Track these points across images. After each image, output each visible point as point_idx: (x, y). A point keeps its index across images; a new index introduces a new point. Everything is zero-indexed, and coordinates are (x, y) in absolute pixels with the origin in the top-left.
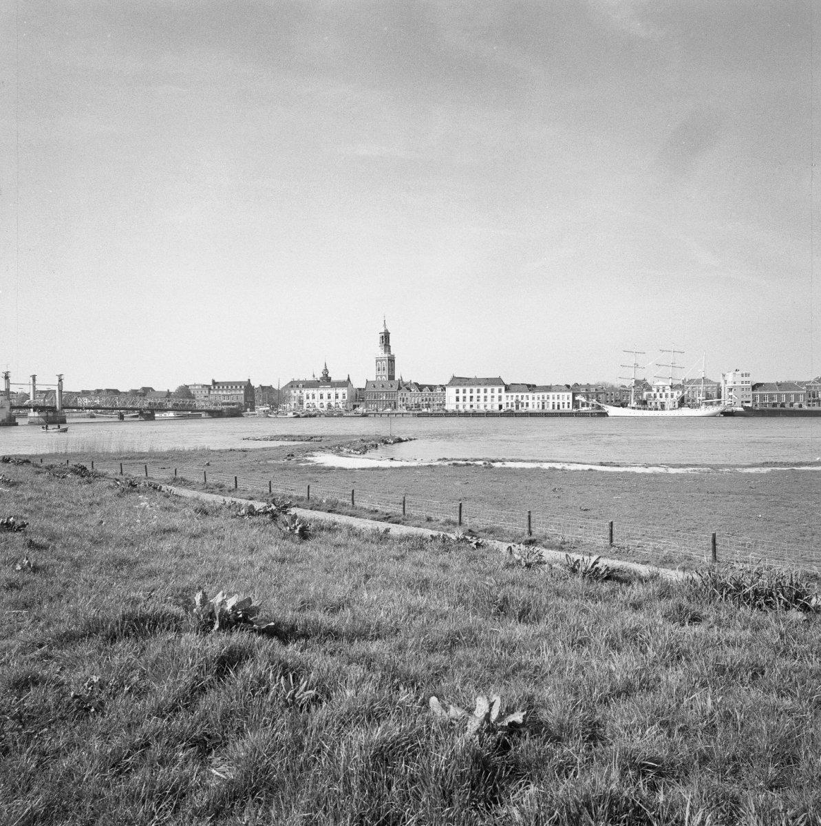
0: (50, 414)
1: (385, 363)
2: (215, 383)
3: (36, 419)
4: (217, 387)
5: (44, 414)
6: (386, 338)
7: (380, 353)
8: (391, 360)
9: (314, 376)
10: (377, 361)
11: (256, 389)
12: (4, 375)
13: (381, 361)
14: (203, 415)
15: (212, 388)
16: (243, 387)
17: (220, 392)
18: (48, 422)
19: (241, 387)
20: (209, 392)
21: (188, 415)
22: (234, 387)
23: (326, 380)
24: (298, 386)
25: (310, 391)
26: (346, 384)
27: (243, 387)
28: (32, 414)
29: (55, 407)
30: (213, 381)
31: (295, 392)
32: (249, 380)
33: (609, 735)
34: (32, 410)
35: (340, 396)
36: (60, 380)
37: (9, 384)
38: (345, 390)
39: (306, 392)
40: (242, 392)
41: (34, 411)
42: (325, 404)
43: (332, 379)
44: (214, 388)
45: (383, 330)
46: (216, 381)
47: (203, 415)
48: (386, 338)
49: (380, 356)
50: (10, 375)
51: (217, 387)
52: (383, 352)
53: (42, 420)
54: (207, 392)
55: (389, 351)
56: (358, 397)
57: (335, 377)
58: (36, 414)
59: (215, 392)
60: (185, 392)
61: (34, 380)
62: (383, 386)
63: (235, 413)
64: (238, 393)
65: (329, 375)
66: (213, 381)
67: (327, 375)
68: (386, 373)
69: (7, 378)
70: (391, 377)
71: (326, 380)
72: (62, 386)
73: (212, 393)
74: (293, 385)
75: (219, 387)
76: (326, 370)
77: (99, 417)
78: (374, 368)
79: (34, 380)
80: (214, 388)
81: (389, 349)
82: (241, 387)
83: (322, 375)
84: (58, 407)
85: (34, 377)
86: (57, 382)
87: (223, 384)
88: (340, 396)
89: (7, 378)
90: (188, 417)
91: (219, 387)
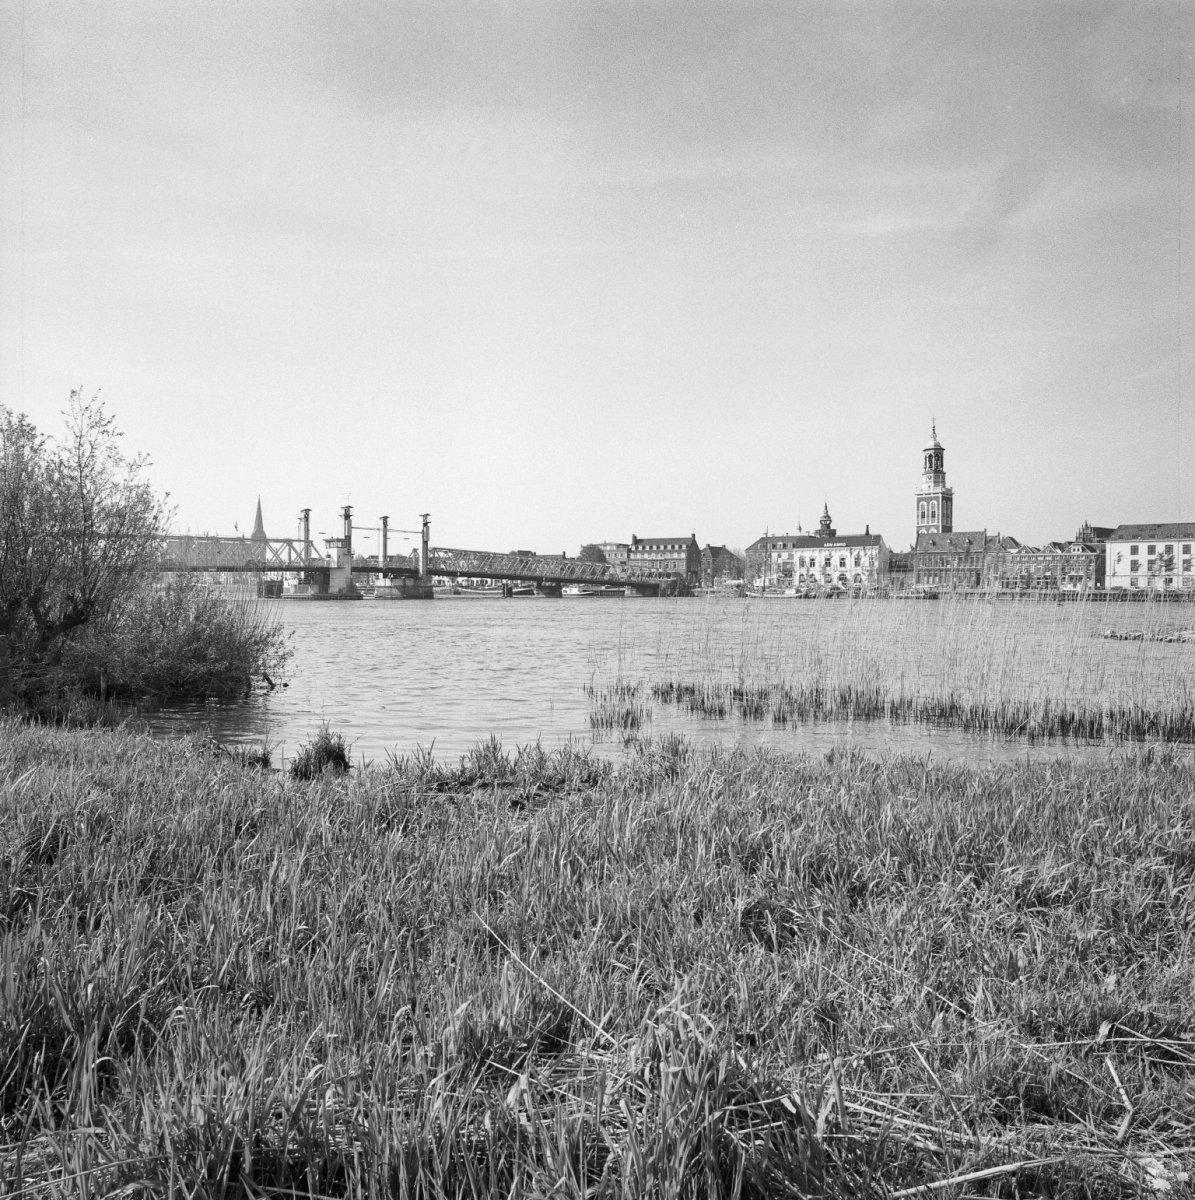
0: (410, 583)
1: (937, 505)
2: (637, 541)
3: (388, 591)
4: (640, 548)
5: (399, 582)
6: (936, 458)
7: (926, 485)
8: (947, 498)
9: (800, 529)
10: (919, 501)
11: (703, 551)
12: (343, 512)
13: (928, 500)
14: (628, 592)
15: (633, 549)
16: (684, 547)
17: (646, 556)
18: (408, 594)
19: (680, 547)
20: (628, 556)
21: (601, 592)
22: (669, 547)
23: (826, 535)
24: (774, 546)
25: (807, 554)
26: (868, 540)
27: (684, 547)
28: (382, 582)
29: (417, 571)
30: (635, 537)
31: (779, 556)
32: (694, 535)
33: (616, 774)
34: (381, 575)
35: (865, 561)
36: (425, 524)
37: (350, 527)
38: (874, 551)
39: (798, 554)
40: (683, 556)
41: (385, 577)
42: (835, 576)
43: (839, 534)
44: (637, 548)
45: (931, 444)
46: (638, 538)
47: (628, 592)
48: (936, 458)
49: (925, 490)
50: (352, 511)
51: (640, 548)
52: (932, 484)
53: (395, 592)
54: (626, 555)
55: (944, 482)
56: (896, 565)
57: (842, 528)
58: (388, 583)
59: (639, 556)
60: (594, 553)
61: (385, 524)
62: (934, 544)
63: (682, 588)
64: (675, 556)
65: (832, 527)
66: (635, 537)
67: (828, 526)
68: (938, 522)
69: (347, 517)
70: (947, 529)
71: (826, 535)
72: (428, 534)
73: (632, 556)
74: (767, 543)
75: (644, 548)
76: (828, 517)
77: (466, 593)
78: (914, 512)
79: (385, 524)
80: (637, 548)
81: (944, 478)
82: (680, 547)
83: (819, 527)
84: (421, 571)
85: (385, 519)
86: (420, 528)
87: (651, 542)
88: (865, 561)
89: (347, 517)
90: (602, 594)
91: (644, 548)
